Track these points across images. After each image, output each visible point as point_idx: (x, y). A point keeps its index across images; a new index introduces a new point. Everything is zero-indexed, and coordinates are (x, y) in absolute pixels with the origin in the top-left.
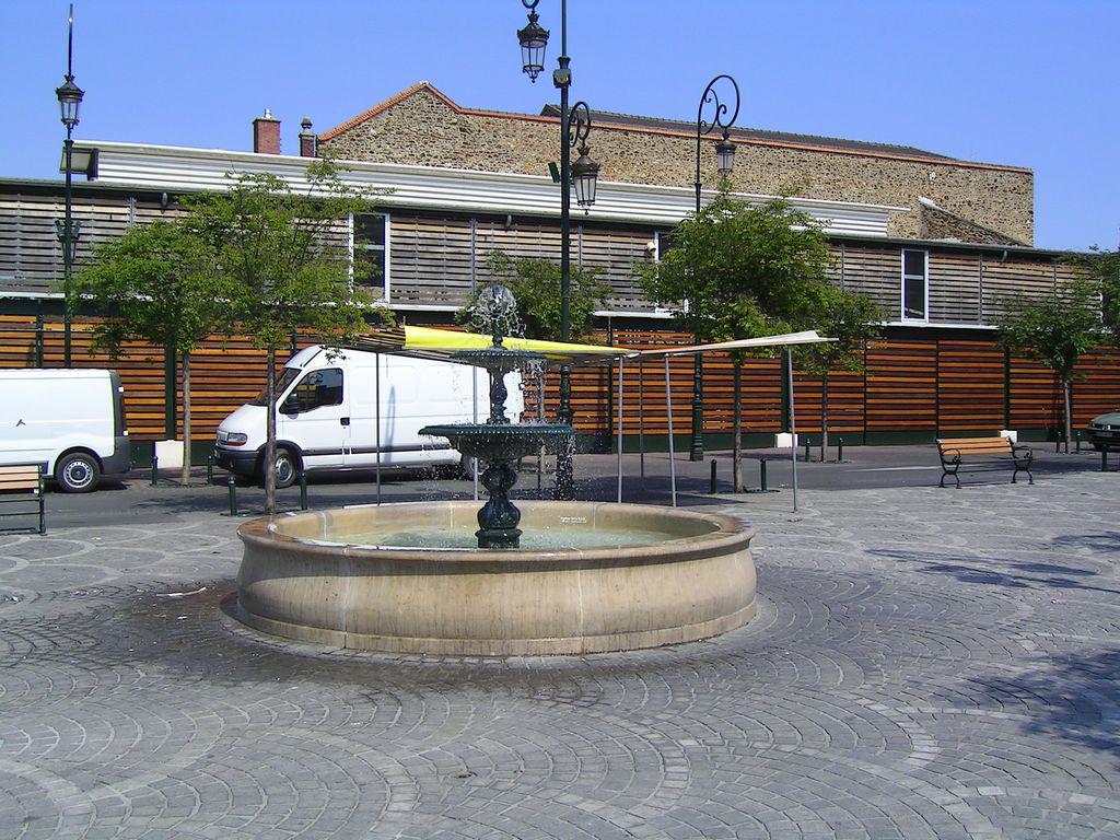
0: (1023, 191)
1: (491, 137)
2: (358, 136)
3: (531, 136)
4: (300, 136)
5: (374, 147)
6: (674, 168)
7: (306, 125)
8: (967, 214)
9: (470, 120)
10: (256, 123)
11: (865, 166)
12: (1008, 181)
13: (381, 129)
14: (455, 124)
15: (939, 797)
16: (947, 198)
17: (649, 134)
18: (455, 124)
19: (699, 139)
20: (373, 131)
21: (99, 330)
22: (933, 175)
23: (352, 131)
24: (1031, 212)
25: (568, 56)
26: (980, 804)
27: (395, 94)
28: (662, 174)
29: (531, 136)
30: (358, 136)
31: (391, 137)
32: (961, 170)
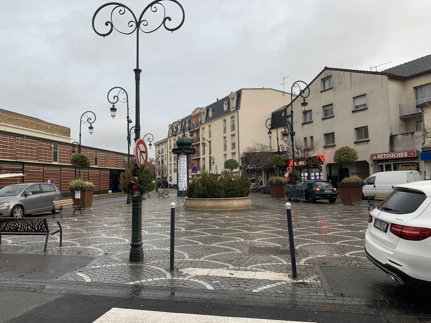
22: (49, 127)
32: (55, 127)
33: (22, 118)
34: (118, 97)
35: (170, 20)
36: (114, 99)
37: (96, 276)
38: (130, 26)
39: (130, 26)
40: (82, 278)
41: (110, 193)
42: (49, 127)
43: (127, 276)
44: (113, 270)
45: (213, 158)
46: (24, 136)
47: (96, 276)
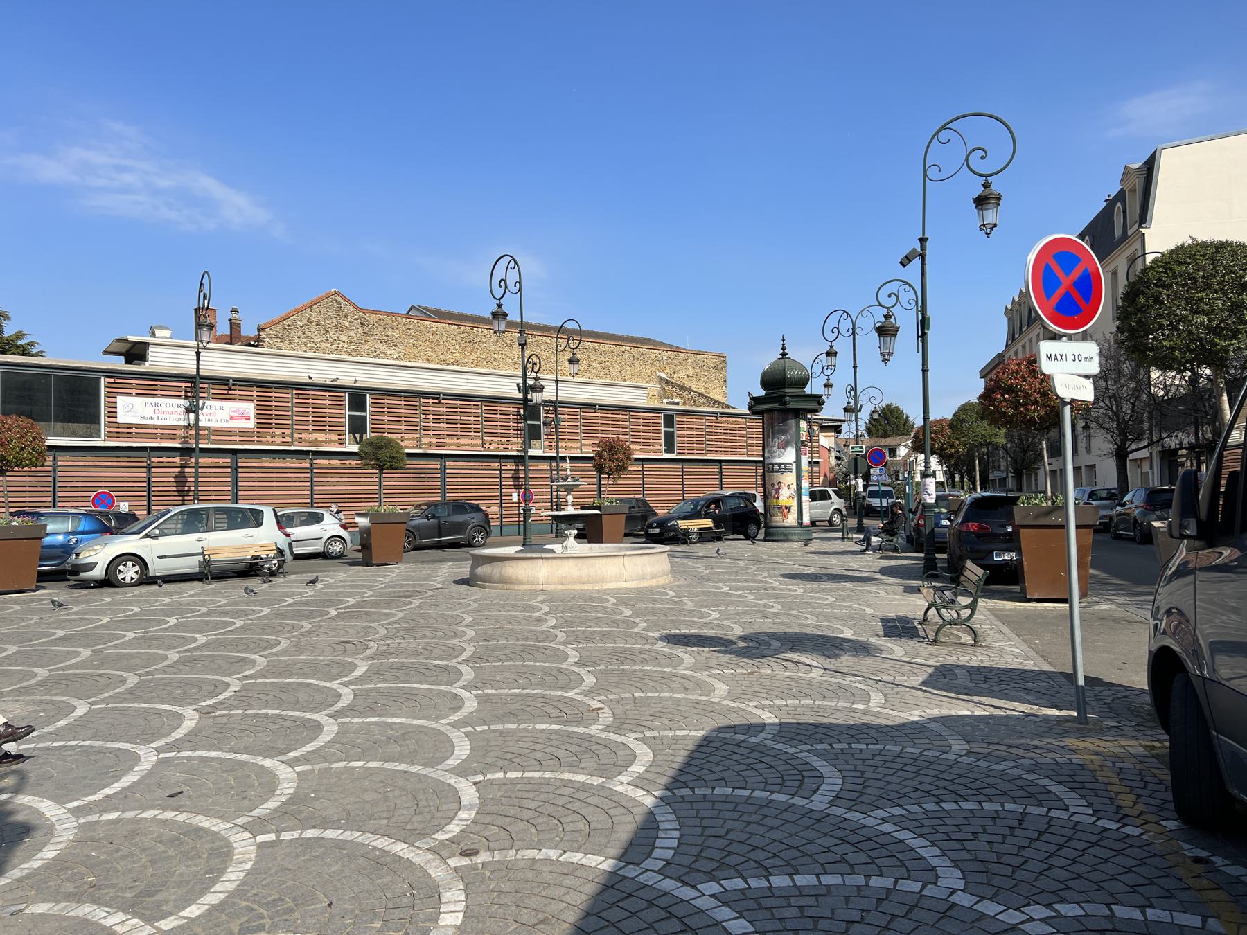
0: (720, 368)
1: (382, 329)
2: (289, 326)
3: (409, 329)
4: (230, 320)
5: (300, 333)
6: (504, 352)
7: (235, 311)
8: (687, 383)
9: (367, 316)
10: (196, 311)
11: (624, 352)
12: (711, 361)
13: (305, 321)
14: (357, 319)
15: (686, 893)
16: (674, 373)
17: (487, 329)
18: (357, 319)
19: (557, 337)
20: (299, 323)
21: (77, 555)
22: (665, 358)
23: (284, 322)
24: (725, 381)
25: (926, 236)
26: (723, 899)
27: (314, 297)
28: (496, 356)
29: (409, 329)
30: (289, 326)
31: (312, 327)
32: (682, 355)
33: (596, 344)
34: (897, 297)
35: (983, 158)
36: (889, 296)
37: (1084, 769)
38: (985, 152)
39: (985, 152)
40: (1061, 800)
41: (112, 406)
42: (665, 358)
43: (741, 763)
44: (867, 769)
45: (873, 392)
46: (228, 380)
47: (1084, 769)
